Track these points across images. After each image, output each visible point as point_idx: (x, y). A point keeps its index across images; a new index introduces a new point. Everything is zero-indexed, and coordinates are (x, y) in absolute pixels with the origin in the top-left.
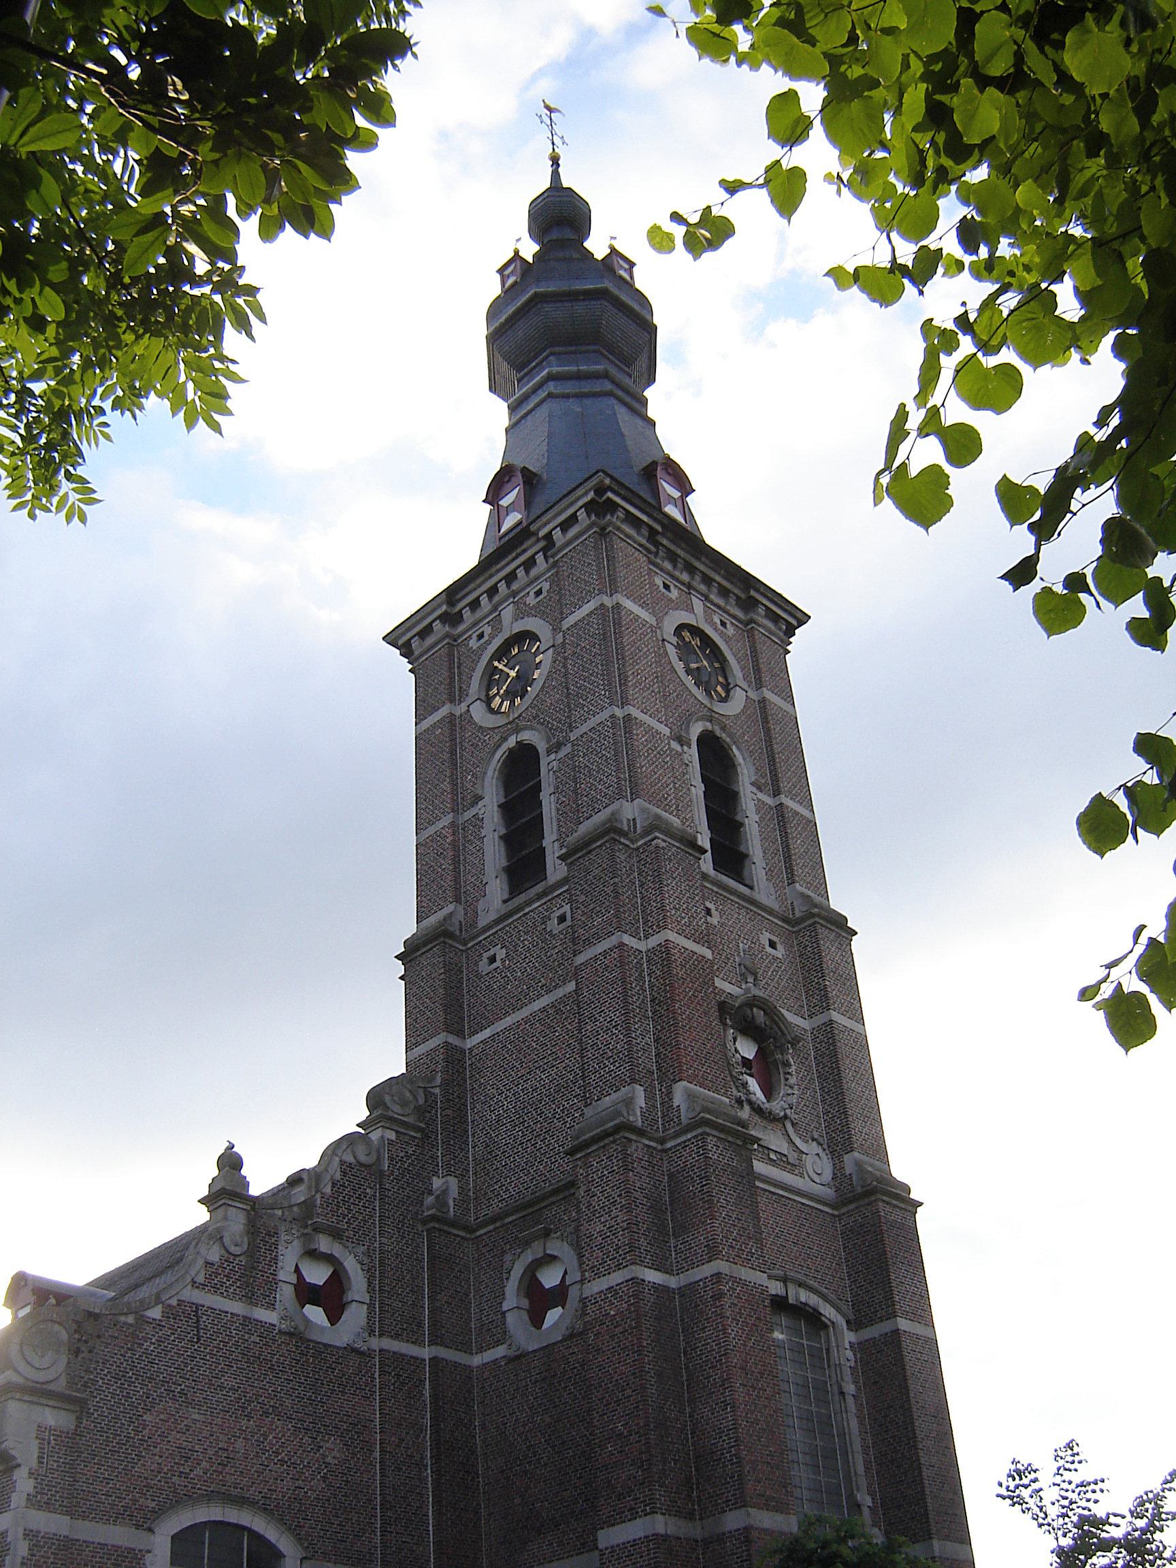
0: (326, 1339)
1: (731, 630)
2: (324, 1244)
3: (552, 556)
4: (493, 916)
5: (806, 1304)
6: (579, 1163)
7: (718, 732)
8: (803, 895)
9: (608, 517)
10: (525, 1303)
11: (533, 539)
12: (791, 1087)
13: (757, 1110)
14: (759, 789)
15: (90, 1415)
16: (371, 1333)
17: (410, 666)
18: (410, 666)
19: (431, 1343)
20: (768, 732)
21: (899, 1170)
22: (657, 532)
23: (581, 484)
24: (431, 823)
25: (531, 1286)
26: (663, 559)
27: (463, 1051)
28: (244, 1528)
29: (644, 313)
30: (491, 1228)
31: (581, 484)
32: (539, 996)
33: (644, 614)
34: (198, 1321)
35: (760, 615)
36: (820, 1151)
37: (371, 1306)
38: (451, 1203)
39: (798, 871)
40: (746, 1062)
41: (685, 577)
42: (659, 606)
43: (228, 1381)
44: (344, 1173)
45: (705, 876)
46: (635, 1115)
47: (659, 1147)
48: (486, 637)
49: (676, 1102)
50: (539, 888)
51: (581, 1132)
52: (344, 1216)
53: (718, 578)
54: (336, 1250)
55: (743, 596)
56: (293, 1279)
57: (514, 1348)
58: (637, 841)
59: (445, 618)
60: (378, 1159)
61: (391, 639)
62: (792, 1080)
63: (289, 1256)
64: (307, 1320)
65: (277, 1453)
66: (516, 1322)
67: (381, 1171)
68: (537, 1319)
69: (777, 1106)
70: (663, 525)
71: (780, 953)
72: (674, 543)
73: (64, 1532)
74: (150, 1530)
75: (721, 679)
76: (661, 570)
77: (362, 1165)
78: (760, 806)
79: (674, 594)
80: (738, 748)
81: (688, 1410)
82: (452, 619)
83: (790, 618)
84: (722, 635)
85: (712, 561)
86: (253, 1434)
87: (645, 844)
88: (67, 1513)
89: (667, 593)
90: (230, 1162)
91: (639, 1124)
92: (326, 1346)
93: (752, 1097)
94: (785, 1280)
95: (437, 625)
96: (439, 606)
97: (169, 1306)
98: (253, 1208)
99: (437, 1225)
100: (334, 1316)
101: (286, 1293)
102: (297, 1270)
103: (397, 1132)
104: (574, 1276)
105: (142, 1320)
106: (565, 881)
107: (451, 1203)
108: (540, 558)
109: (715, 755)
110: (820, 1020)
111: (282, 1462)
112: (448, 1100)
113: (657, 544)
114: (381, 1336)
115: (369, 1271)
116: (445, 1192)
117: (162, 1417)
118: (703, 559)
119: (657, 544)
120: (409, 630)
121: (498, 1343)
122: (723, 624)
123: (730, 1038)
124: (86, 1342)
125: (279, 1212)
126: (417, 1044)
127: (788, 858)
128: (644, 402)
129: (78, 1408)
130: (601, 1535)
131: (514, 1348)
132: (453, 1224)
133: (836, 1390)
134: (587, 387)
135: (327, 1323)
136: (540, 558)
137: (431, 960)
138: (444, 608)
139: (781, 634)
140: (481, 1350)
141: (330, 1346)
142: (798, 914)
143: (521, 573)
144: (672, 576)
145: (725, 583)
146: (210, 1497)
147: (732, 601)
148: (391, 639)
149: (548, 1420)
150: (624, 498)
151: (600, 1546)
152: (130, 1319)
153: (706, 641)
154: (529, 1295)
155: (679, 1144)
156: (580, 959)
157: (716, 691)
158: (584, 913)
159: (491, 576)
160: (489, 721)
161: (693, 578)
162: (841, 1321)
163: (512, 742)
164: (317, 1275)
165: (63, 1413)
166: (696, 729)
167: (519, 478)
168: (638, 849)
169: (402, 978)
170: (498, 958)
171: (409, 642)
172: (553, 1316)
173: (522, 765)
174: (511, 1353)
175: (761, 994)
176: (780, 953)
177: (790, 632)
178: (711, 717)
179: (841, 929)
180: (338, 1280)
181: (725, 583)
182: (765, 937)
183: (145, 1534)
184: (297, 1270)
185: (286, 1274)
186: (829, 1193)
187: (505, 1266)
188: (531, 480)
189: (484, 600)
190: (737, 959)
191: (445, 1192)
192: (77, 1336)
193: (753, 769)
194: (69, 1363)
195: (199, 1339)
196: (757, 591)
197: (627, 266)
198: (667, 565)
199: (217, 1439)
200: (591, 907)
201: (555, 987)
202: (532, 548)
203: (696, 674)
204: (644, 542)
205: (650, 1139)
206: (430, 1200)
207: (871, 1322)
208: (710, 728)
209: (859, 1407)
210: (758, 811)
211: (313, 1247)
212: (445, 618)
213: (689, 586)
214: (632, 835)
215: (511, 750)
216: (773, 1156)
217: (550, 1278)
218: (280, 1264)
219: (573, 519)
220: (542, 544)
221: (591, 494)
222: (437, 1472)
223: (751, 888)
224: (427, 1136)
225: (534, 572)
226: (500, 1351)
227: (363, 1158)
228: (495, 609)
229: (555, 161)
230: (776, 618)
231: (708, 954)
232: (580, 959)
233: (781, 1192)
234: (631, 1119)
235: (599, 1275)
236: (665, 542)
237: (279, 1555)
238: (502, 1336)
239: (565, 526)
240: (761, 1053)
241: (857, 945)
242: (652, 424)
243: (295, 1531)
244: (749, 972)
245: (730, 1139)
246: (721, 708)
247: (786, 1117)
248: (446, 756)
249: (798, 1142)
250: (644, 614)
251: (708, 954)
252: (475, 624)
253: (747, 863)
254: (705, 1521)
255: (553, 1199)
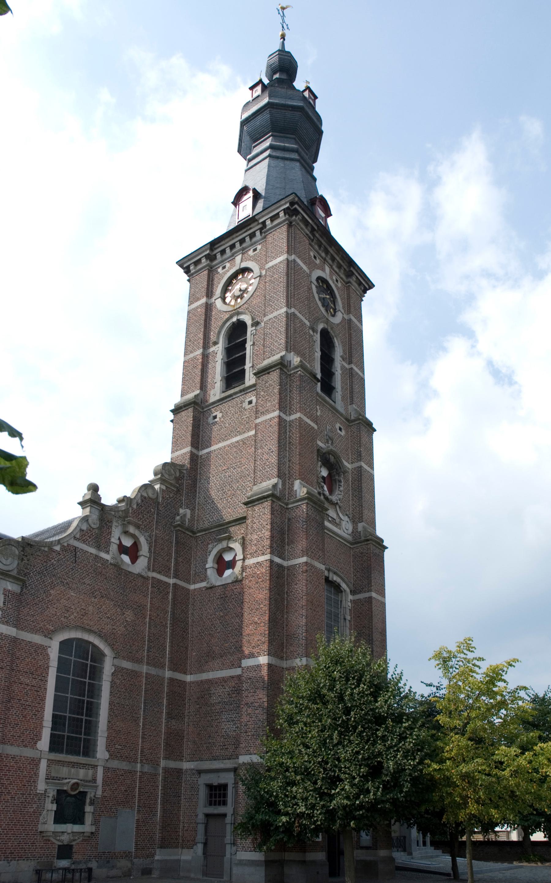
0: (130, 570)
1: (339, 285)
2: (132, 529)
3: (265, 233)
4: (217, 397)
5: (335, 581)
6: (249, 509)
7: (329, 330)
8: (356, 410)
9: (294, 217)
10: (216, 566)
11: (256, 223)
12: (341, 491)
13: (327, 498)
14: (343, 360)
15: (26, 587)
16: (149, 569)
17: (188, 278)
18: (188, 278)
19: (174, 577)
20: (350, 335)
21: (380, 532)
22: (315, 230)
23: (284, 198)
24: (191, 352)
25: (219, 560)
26: (315, 243)
27: (197, 456)
28: (90, 643)
29: (318, 123)
30: (204, 533)
31: (284, 198)
32: (236, 435)
33: (305, 267)
34: (76, 554)
35: (353, 280)
36: (349, 520)
37: (149, 559)
38: (187, 521)
39: (355, 399)
40: (323, 478)
41: (323, 255)
42: (312, 266)
43: (87, 581)
44: (142, 501)
45: (317, 393)
46: (277, 491)
47: (285, 507)
48: (227, 268)
49: (295, 488)
50: (242, 387)
51: (252, 496)
52: (141, 519)
53: (338, 258)
54: (137, 533)
55: (347, 270)
56: (118, 542)
57: (209, 583)
58: (291, 371)
59: (207, 257)
60: (158, 496)
61: (180, 263)
62: (342, 489)
63: (116, 533)
64: (122, 560)
65: (106, 614)
66: (211, 573)
67: (159, 503)
68: (220, 573)
69: (334, 498)
70: (318, 227)
71: (343, 433)
72: (322, 237)
73: (14, 634)
74: (51, 638)
75: (332, 305)
76: (314, 248)
77: (150, 498)
78: (343, 367)
79: (318, 261)
80: (337, 339)
81: (285, 616)
82: (211, 258)
83: (366, 285)
84: (336, 286)
85: (337, 250)
86: (96, 605)
87: (294, 373)
88: (15, 627)
89: (315, 260)
90: (94, 488)
91: (278, 495)
92: (130, 572)
93: (325, 492)
94: (329, 570)
95: (204, 260)
96: (206, 250)
97: (63, 546)
98: (102, 510)
99: (180, 529)
100: (134, 559)
101: (114, 548)
102: (119, 539)
103: (166, 486)
104: (240, 556)
105: (51, 550)
106: (254, 385)
107: (187, 521)
108: (258, 233)
109: (327, 340)
110: (356, 465)
111: (108, 618)
112: (190, 477)
113: (314, 236)
114: (153, 571)
115: (150, 544)
116: (185, 515)
117: (58, 592)
118: (333, 248)
119: (314, 236)
120: (189, 260)
121: (202, 581)
122: (337, 281)
123: (319, 465)
124: (26, 556)
125: (113, 513)
126: (177, 450)
127: (352, 392)
128: (312, 169)
129: (21, 584)
130: (243, 661)
131: (209, 583)
132: (187, 529)
133: (342, 617)
134: (287, 155)
135: (130, 563)
136: (258, 233)
137: (188, 415)
138: (208, 252)
139: (361, 291)
140: (194, 583)
141: (131, 573)
142: (352, 418)
143: (248, 239)
144: (318, 253)
145: (340, 261)
146: (76, 628)
147: (342, 271)
148: (180, 263)
149: (222, 614)
150: (303, 210)
151: (242, 666)
152: (46, 549)
153: (329, 287)
154: (218, 563)
155: (295, 506)
156: (258, 421)
157: (330, 311)
158: (262, 400)
159: (233, 239)
160: (225, 308)
161: (327, 256)
162: (348, 590)
163: (234, 319)
164: (128, 542)
165: (14, 584)
166: (321, 326)
167: (251, 194)
168: (291, 374)
169: (172, 421)
170: (218, 417)
171: (188, 267)
172: (228, 572)
173: (237, 331)
174: (208, 586)
175: (334, 449)
176: (343, 433)
177: (365, 292)
178: (327, 322)
179: (370, 428)
180: (136, 546)
181: (340, 261)
182: (338, 426)
183: (49, 640)
184: (119, 539)
185: (114, 540)
186: (350, 538)
187: (209, 550)
188: (257, 196)
189: (228, 250)
190: (326, 433)
191: (185, 515)
192: (22, 553)
193: (342, 351)
194: (18, 564)
195: (76, 562)
196: (354, 268)
197: (313, 98)
198: (316, 247)
199: (81, 605)
200: (266, 398)
201: (244, 432)
202: (255, 227)
203: (323, 300)
204: (308, 233)
205: (283, 503)
206: (178, 518)
207: (360, 592)
208: (326, 327)
209: (351, 625)
210: (341, 369)
211: (127, 530)
212: (207, 257)
213: (325, 260)
214: (288, 368)
215: (233, 323)
216: (330, 519)
217: (228, 557)
218: (112, 535)
219: (277, 216)
220: (260, 226)
221: (288, 205)
222: (173, 630)
223: (335, 402)
224: (178, 491)
225: (254, 240)
226: (203, 584)
227: (151, 495)
228: (233, 255)
229: (283, 37)
230: (360, 284)
231: (316, 427)
232: (258, 421)
233: (331, 534)
234: (275, 492)
235: (253, 557)
236: (317, 235)
237: (104, 655)
238: (205, 578)
239: (273, 219)
240: (330, 475)
241: (376, 436)
242: (315, 179)
243: (112, 646)
244: (329, 439)
245: (317, 507)
246: (332, 319)
247: (337, 503)
248: (202, 322)
249: (341, 515)
250: (305, 267)
251: (316, 427)
252: (222, 261)
253: (334, 391)
254: (288, 661)
255: (234, 524)
